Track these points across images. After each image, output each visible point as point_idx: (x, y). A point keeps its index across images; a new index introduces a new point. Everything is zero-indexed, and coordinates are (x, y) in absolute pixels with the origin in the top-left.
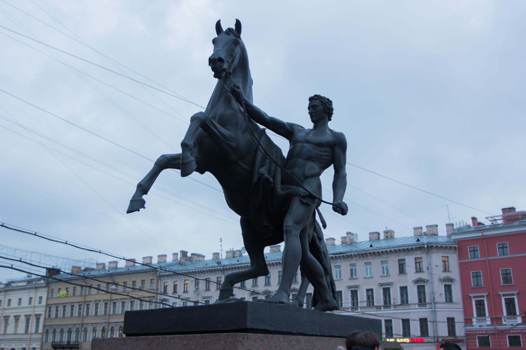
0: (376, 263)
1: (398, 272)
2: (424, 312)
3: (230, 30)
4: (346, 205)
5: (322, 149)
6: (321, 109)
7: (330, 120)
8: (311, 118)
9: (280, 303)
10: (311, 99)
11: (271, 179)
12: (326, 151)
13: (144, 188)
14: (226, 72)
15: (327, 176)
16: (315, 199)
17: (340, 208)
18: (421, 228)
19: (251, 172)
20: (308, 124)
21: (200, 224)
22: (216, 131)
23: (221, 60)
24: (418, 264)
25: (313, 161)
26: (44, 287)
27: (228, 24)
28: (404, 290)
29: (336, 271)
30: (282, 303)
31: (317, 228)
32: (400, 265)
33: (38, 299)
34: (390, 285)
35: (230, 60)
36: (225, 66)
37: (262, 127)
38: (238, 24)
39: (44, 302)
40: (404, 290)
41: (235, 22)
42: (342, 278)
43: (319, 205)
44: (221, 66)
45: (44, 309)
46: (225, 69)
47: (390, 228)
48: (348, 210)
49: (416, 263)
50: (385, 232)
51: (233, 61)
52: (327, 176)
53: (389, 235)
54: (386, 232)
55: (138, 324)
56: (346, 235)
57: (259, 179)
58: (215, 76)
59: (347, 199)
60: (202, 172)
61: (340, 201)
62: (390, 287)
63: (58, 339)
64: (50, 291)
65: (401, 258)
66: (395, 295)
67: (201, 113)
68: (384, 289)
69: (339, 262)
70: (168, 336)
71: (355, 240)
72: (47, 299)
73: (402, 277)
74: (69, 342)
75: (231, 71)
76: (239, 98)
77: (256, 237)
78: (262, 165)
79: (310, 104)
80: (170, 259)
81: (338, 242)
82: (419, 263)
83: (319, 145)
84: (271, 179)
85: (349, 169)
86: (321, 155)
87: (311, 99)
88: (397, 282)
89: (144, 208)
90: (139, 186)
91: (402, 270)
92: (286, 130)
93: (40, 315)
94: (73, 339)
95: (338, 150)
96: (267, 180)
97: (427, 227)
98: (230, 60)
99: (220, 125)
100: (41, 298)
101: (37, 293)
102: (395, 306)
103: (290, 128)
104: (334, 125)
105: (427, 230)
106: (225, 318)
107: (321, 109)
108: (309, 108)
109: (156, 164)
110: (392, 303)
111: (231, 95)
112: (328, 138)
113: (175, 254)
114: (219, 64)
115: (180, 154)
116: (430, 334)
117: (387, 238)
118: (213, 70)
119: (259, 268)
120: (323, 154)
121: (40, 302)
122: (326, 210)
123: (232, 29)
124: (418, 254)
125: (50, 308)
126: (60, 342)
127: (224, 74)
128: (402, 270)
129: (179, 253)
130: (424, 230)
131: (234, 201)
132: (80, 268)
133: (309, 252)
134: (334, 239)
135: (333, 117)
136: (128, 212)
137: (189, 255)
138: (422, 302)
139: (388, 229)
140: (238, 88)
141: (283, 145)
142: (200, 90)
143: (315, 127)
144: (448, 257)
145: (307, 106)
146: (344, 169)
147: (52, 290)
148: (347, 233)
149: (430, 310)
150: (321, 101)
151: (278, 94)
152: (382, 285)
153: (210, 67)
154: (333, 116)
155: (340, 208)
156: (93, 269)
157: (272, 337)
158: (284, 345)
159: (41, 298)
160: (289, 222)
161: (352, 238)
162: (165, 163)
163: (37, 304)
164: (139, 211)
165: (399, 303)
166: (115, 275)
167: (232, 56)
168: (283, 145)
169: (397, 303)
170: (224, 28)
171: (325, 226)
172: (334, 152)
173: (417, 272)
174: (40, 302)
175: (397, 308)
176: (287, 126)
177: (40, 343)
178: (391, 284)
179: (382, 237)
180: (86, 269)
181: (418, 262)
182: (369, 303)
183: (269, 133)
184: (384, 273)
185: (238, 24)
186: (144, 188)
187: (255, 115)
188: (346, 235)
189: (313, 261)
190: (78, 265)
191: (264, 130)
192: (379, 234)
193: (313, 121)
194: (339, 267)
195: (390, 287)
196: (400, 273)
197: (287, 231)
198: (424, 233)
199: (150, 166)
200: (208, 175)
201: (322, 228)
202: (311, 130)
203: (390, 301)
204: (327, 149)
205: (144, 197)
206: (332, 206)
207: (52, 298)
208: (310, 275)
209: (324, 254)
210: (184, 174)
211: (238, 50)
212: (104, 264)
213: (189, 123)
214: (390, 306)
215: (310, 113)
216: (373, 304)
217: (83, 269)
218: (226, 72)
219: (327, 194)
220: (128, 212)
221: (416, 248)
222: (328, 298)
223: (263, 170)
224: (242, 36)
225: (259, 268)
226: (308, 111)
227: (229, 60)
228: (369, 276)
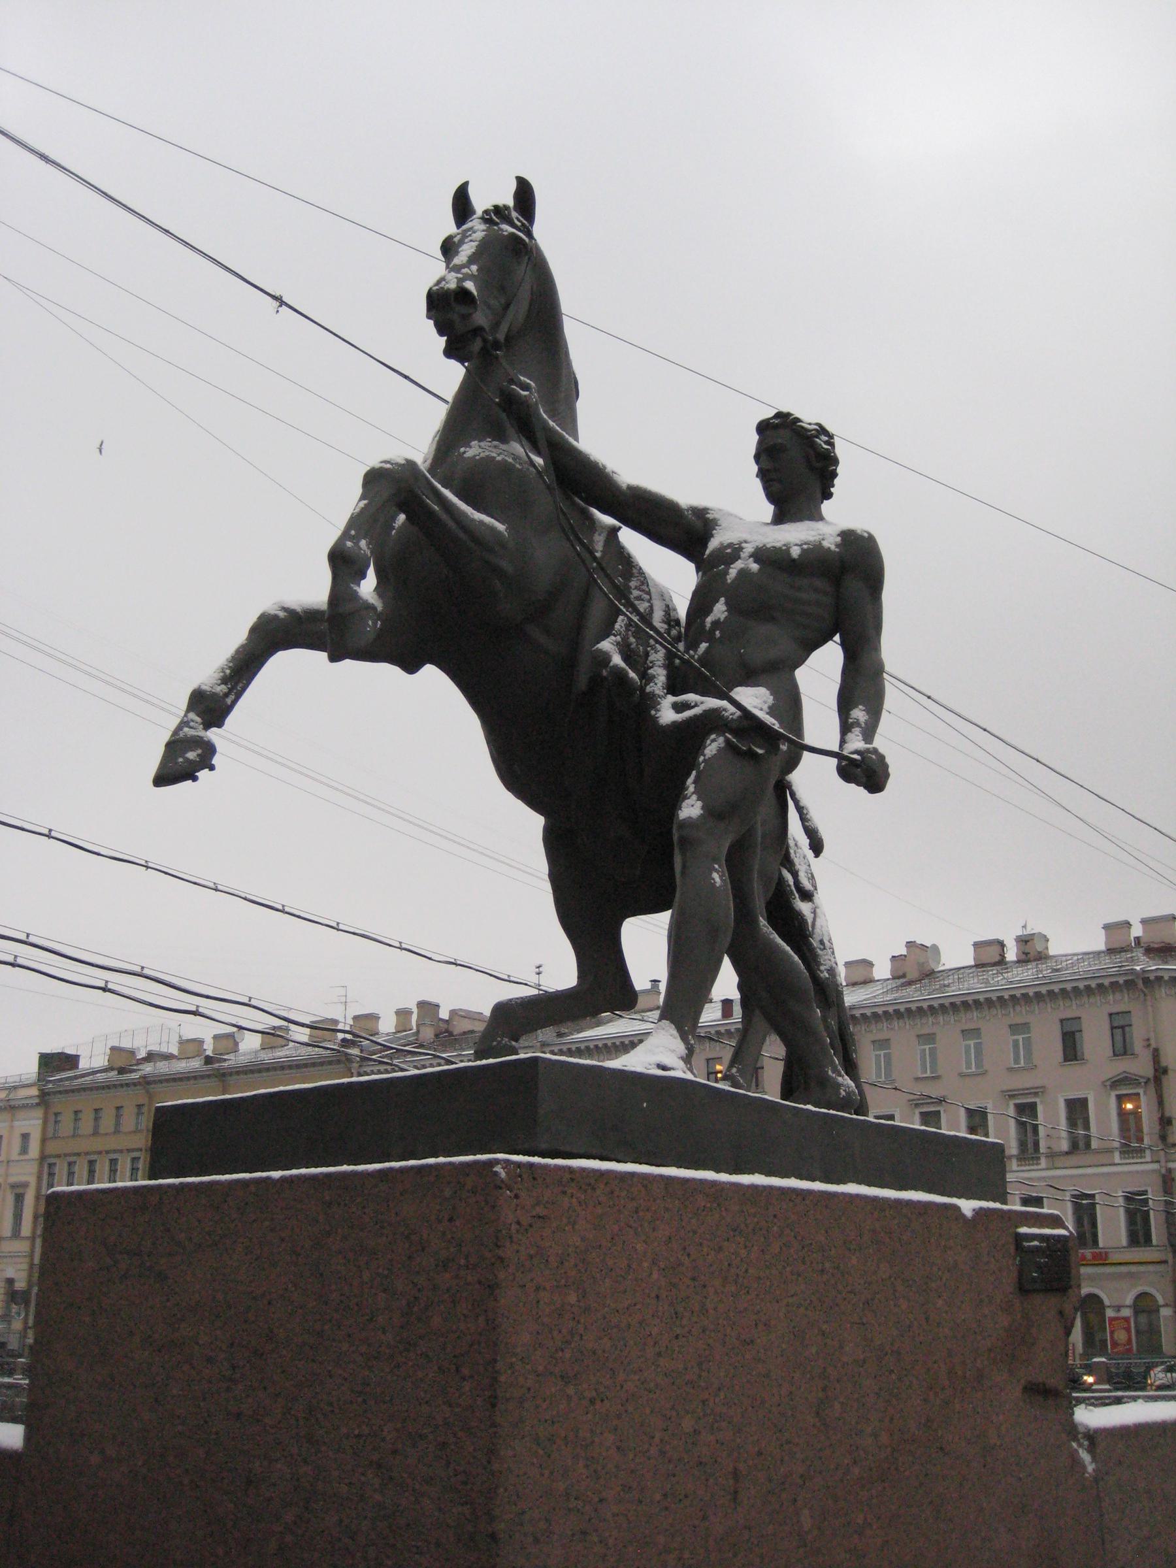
0: (995, 1030)
1: (1060, 1055)
3: (499, 212)
6: (796, 461)
7: (828, 495)
8: (766, 488)
10: (763, 427)
12: (816, 590)
13: (211, 707)
14: (485, 341)
15: (821, 672)
17: (866, 772)
18: (1128, 924)
19: (570, 663)
22: (451, 524)
23: (462, 295)
24: (1118, 1032)
25: (773, 619)
26: (32, 1106)
27: (493, 193)
28: (1077, 1109)
29: (878, 1056)
34: (1036, 1094)
35: (500, 308)
36: (480, 318)
37: (608, 520)
38: (524, 194)
39: (34, 1150)
40: (1077, 1109)
41: (513, 186)
43: (792, 763)
44: (465, 317)
45: (33, 1168)
47: (1034, 928)
48: (887, 776)
49: (1112, 1028)
51: (507, 306)
53: (1032, 949)
54: (1024, 941)
57: (596, 681)
58: (449, 352)
62: (1037, 1100)
64: (52, 1118)
65: (1069, 1014)
66: (1052, 1121)
68: (1021, 1109)
69: (881, 1031)
71: (933, 965)
72: (44, 1141)
73: (1074, 1071)
75: (501, 336)
76: (526, 426)
78: (606, 633)
79: (760, 443)
80: (387, 1025)
81: (883, 971)
82: (1123, 1027)
85: (895, 647)
87: (763, 427)
88: (1060, 1087)
89: (212, 768)
91: (1071, 1049)
92: (684, 530)
93: (25, 1185)
95: (854, 585)
96: (619, 675)
97: (1144, 922)
98: (500, 308)
100: (25, 1137)
101: (16, 1123)
102: (1052, 1155)
103: (699, 524)
104: (842, 512)
105: (1144, 931)
107: (796, 461)
108: (757, 458)
109: (254, 630)
110: (1043, 1149)
111: (504, 416)
113: (403, 1014)
114: (463, 310)
116: (1154, 1242)
117: (1025, 959)
118: (441, 332)
119: (604, 982)
121: (24, 1150)
122: (814, 781)
123: (506, 207)
124: (1120, 1002)
125: (51, 1166)
127: (477, 345)
128: (1071, 1049)
129: (415, 1010)
130: (1137, 931)
131: (523, 762)
132: (132, 1053)
133: (763, 922)
134: (869, 964)
135: (839, 486)
136: (163, 779)
137: (444, 1014)
139: (1028, 931)
141: (671, 576)
142: (403, 401)
145: (753, 451)
146: (877, 648)
147: (56, 1114)
149: (1155, 1166)
150: (794, 431)
151: (658, 417)
152: (1012, 1097)
153: (431, 322)
154: (836, 481)
155: (866, 772)
156: (168, 1057)
158: (667, 1209)
159: (25, 1137)
161: (922, 960)
162: (276, 633)
163: (15, 1155)
164: (195, 779)
165: (1065, 1146)
166: (231, 1074)
167: (502, 289)
168: (671, 576)
169: (1056, 1149)
170: (481, 202)
171: (817, 846)
172: (840, 593)
173: (1115, 1055)
174: (24, 1150)
175: (1058, 1164)
176: (689, 514)
177: (25, 1266)
178: (1038, 1091)
179: (1011, 955)
180: (151, 1057)
181: (1119, 1027)
183: (632, 540)
184: (1017, 1061)
185: (524, 194)
186: (211, 707)
187: (582, 482)
190: (126, 1044)
192: (1001, 944)
193: (771, 497)
194: (883, 1044)
195: (1037, 1100)
196: (1066, 1059)
197: (684, 841)
198: (1137, 939)
199: (237, 636)
200: (433, 680)
203: (1036, 1145)
204: (819, 583)
206: (834, 762)
207: (55, 1137)
211: (522, 271)
212: (200, 1042)
214: (1038, 1158)
215: (763, 474)
217: (142, 1054)
218: (485, 341)
219: (820, 722)
220: (163, 779)
221: (1112, 984)
224: (540, 230)
226: (755, 468)
228: (928, 1074)
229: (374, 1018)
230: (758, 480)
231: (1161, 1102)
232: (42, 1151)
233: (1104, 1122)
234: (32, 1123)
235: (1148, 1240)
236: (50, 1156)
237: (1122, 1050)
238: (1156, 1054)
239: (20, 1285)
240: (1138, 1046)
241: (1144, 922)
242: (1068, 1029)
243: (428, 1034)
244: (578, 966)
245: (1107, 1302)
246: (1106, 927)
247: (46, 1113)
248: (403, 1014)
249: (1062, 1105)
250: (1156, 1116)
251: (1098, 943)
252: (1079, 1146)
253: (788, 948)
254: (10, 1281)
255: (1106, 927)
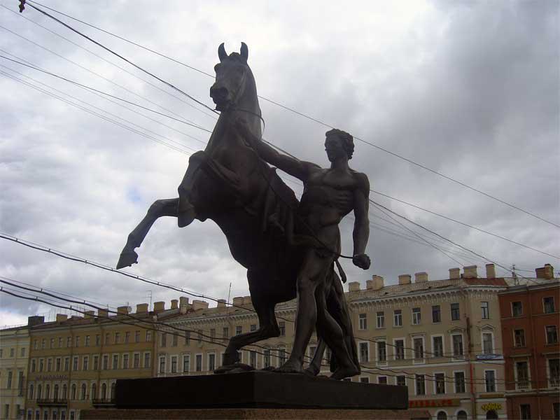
2: (459, 364)
3: (234, 54)
4: (368, 257)
5: (342, 193)
7: (351, 158)
9: (291, 372)
11: (283, 229)
13: (136, 238)
15: (346, 226)
16: (333, 252)
17: (361, 261)
20: (325, 163)
21: (208, 270)
23: (224, 90)
27: (232, 48)
28: (438, 341)
30: (295, 372)
31: (336, 279)
32: (433, 312)
33: (20, 350)
36: (229, 97)
37: (271, 166)
38: (244, 48)
42: (364, 335)
45: (26, 362)
46: (230, 100)
50: (416, 275)
52: (346, 226)
55: (132, 393)
56: (372, 279)
59: (368, 251)
60: (203, 220)
61: (361, 253)
63: (44, 397)
67: (201, 152)
69: (363, 310)
70: (165, 410)
74: (56, 400)
75: (236, 102)
77: (265, 293)
83: (338, 188)
84: (283, 229)
85: (373, 214)
86: (341, 200)
87: (328, 134)
90: (131, 237)
94: (61, 396)
98: (233, 82)
99: (225, 166)
104: (355, 164)
106: (231, 386)
112: (348, 180)
115: (177, 199)
116: (466, 391)
119: (270, 328)
120: (341, 198)
121: (23, 355)
123: (238, 53)
126: (46, 400)
130: (462, 272)
132: (66, 316)
133: (326, 311)
135: (354, 155)
136: (223, 44)
137: (191, 302)
138: (458, 352)
140: (244, 122)
142: (197, 127)
143: (333, 166)
144: (427, 412)
148: (374, 276)
151: (291, 123)
153: (212, 99)
155: (361, 261)
157: (282, 412)
160: (304, 279)
162: (160, 209)
164: (130, 266)
168: (297, 187)
182: (399, 356)
185: (244, 48)
188: (372, 279)
189: (331, 319)
191: (274, 170)
200: (210, 223)
201: (342, 282)
202: (329, 170)
204: (346, 192)
205: (136, 250)
208: (328, 336)
209: (344, 311)
210: (183, 223)
211: (243, 79)
213: (187, 164)
216: (403, 358)
220: (223, 44)
222: (348, 362)
223: (273, 218)
225: (270, 328)
227: (234, 91)
229: (163, 303)
230: (326, 152)
231: (469, 339)
232: (30, 355)
233: (448, 346)
234: (26, 343)
235: (464, 391)
236: (33, 357)
237: (455, 316)
238: (468, 320)
239: (22, 408)
240: (461, 316)
241: (465, 268)
242: (435, 310)
243: (184, 310)
244: (217, 223)
245: (447, 414)
246: (450, 270)
247: (31, 340)
248: (174, 302)
249: (432, 341)
250: (467, 345)
251: (447, 276)
252: (439, 354)
253: (335, 322)
254: (18, 406)
255: (450, 270)
